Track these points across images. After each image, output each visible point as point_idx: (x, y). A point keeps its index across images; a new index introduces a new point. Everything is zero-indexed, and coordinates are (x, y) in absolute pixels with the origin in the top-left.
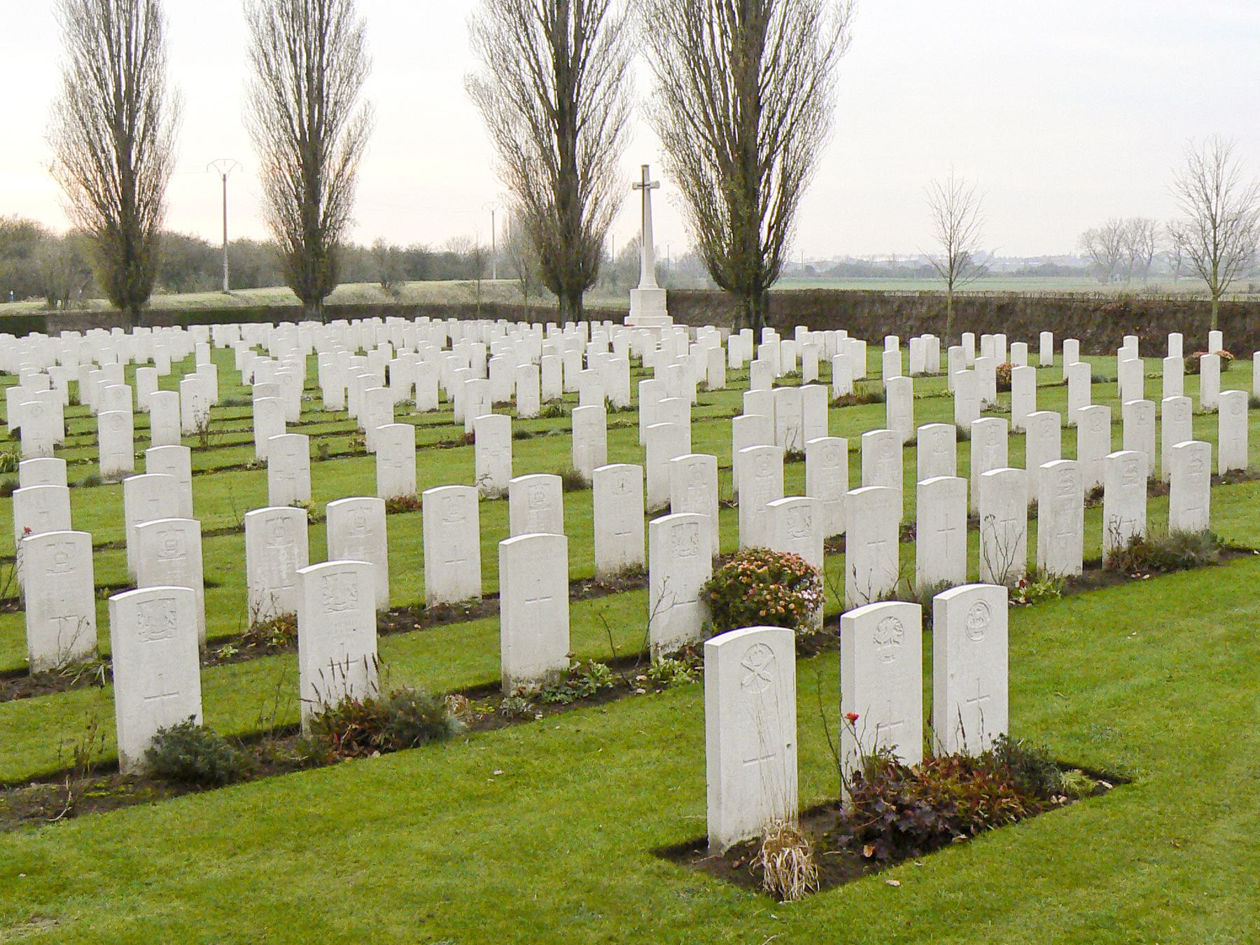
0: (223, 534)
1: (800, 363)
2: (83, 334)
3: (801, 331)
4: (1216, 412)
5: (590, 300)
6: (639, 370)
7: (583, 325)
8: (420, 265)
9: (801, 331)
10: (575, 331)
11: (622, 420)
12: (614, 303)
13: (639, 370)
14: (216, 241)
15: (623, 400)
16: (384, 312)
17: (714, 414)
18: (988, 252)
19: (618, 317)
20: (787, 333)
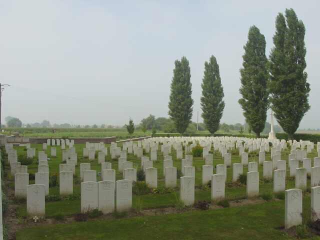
0: (199, 172)
1: (301, 146)
2: (151, 115)
3: (301, 141)
4: (302, 162)
5: (261, 134)
6: (270, 144)
7: (260, 139)
8: (232, 127)
9: (301, 141)
10: (259, 140)
11: (268, 154)
12: (266, 135)
13: (270, 144)
14: (197, 122)
15: (268, 151)
16: (224, 135)
17: (285, 155)
18: (88, 207)
19: (267, 137)
20: (298, 141)
